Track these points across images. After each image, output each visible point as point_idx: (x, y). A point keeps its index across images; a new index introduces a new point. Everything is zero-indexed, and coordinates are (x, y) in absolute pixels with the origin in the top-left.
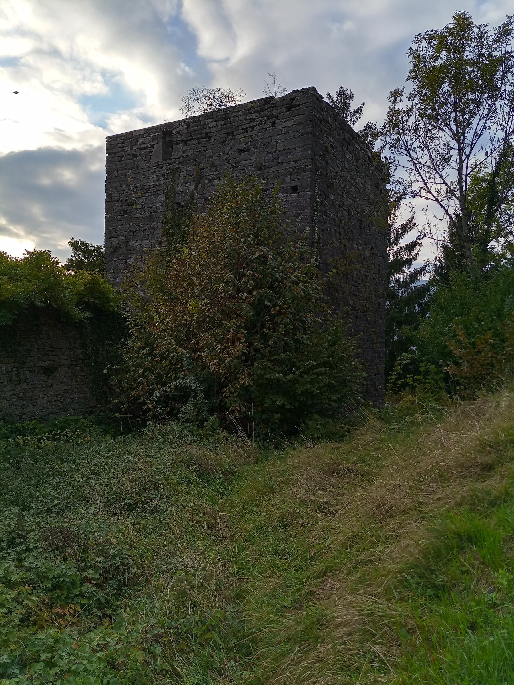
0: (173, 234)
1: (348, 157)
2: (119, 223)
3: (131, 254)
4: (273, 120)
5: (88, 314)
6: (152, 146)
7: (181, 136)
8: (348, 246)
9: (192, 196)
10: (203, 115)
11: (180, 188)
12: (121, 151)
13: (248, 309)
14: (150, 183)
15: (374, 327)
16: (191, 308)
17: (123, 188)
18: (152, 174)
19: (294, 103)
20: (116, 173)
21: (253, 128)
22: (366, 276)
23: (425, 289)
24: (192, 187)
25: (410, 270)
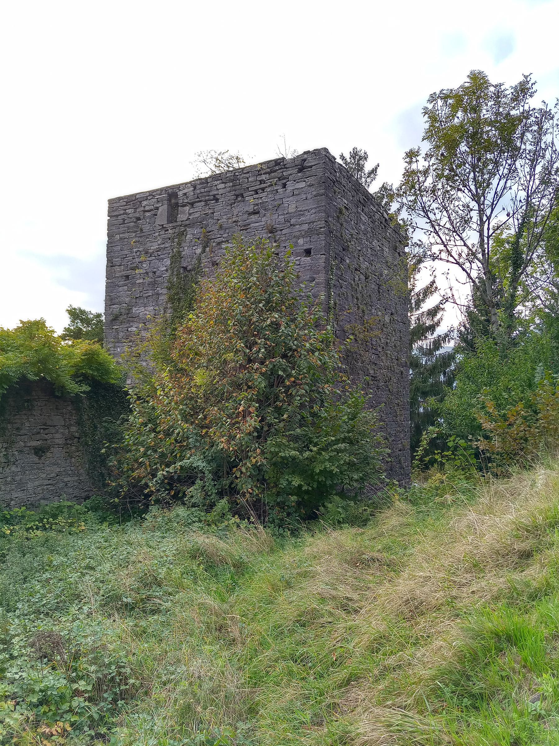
0: (179, 299)
1: (363, 219)
2: (121, 289)
3: (133, 321)
4: (284, 181)
6: (157, 208)
7: (187, 198)
8: (367, 312)
9: (199, 260)
11: (186, 251)
12: (124, 214)
13: (259, 380)
14: (155, 246)
15: (397, 399)
17: (126, 252)
19: (306, 164)
20: (118, 237)
21: (263, 189)
22: (387, 343)
24: (199, 251)
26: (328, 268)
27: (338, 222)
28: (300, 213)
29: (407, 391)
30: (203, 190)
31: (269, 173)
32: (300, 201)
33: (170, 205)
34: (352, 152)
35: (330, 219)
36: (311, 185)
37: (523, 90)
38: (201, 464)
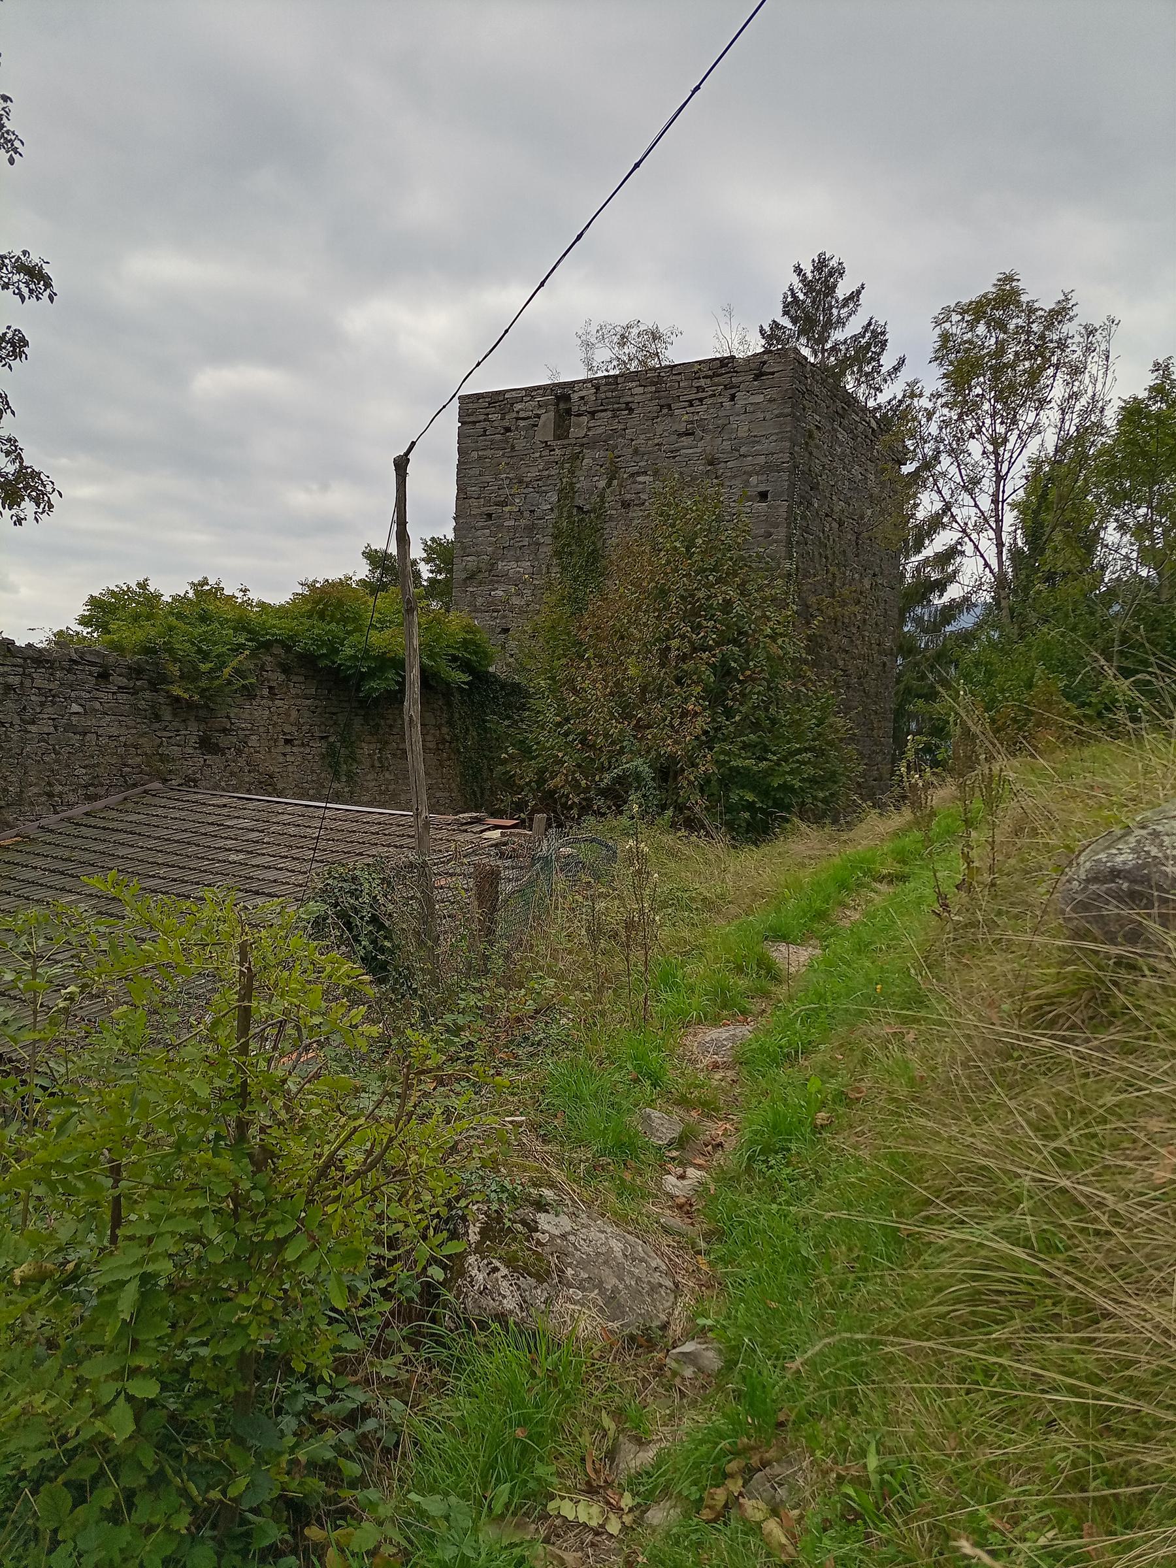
0: (571, 554)
1: (840, 436)
4: (733, 391)
8: (839, 576)
9: (602, 496)
10: (622, 375)
11: (582, 484)
12: (485, 420)
13: (708, 673)
15: (875, 703)
16: (632, 672)
17: (487, 478)
18: (535, 460)
19: (765, 369)
20: (475, 455)
21: (701, 400)
22: (865, 620)
23: (967, 637)
25: (942, 601)
26: (791, 518)
27: (806, 450)
28: (754, 440)
30: (609, 394)
31: (710, 377)
32: (754, 419)
33: (557, 411)
34: (816, 259)
35: (796, 449)
37: (1060, 313)
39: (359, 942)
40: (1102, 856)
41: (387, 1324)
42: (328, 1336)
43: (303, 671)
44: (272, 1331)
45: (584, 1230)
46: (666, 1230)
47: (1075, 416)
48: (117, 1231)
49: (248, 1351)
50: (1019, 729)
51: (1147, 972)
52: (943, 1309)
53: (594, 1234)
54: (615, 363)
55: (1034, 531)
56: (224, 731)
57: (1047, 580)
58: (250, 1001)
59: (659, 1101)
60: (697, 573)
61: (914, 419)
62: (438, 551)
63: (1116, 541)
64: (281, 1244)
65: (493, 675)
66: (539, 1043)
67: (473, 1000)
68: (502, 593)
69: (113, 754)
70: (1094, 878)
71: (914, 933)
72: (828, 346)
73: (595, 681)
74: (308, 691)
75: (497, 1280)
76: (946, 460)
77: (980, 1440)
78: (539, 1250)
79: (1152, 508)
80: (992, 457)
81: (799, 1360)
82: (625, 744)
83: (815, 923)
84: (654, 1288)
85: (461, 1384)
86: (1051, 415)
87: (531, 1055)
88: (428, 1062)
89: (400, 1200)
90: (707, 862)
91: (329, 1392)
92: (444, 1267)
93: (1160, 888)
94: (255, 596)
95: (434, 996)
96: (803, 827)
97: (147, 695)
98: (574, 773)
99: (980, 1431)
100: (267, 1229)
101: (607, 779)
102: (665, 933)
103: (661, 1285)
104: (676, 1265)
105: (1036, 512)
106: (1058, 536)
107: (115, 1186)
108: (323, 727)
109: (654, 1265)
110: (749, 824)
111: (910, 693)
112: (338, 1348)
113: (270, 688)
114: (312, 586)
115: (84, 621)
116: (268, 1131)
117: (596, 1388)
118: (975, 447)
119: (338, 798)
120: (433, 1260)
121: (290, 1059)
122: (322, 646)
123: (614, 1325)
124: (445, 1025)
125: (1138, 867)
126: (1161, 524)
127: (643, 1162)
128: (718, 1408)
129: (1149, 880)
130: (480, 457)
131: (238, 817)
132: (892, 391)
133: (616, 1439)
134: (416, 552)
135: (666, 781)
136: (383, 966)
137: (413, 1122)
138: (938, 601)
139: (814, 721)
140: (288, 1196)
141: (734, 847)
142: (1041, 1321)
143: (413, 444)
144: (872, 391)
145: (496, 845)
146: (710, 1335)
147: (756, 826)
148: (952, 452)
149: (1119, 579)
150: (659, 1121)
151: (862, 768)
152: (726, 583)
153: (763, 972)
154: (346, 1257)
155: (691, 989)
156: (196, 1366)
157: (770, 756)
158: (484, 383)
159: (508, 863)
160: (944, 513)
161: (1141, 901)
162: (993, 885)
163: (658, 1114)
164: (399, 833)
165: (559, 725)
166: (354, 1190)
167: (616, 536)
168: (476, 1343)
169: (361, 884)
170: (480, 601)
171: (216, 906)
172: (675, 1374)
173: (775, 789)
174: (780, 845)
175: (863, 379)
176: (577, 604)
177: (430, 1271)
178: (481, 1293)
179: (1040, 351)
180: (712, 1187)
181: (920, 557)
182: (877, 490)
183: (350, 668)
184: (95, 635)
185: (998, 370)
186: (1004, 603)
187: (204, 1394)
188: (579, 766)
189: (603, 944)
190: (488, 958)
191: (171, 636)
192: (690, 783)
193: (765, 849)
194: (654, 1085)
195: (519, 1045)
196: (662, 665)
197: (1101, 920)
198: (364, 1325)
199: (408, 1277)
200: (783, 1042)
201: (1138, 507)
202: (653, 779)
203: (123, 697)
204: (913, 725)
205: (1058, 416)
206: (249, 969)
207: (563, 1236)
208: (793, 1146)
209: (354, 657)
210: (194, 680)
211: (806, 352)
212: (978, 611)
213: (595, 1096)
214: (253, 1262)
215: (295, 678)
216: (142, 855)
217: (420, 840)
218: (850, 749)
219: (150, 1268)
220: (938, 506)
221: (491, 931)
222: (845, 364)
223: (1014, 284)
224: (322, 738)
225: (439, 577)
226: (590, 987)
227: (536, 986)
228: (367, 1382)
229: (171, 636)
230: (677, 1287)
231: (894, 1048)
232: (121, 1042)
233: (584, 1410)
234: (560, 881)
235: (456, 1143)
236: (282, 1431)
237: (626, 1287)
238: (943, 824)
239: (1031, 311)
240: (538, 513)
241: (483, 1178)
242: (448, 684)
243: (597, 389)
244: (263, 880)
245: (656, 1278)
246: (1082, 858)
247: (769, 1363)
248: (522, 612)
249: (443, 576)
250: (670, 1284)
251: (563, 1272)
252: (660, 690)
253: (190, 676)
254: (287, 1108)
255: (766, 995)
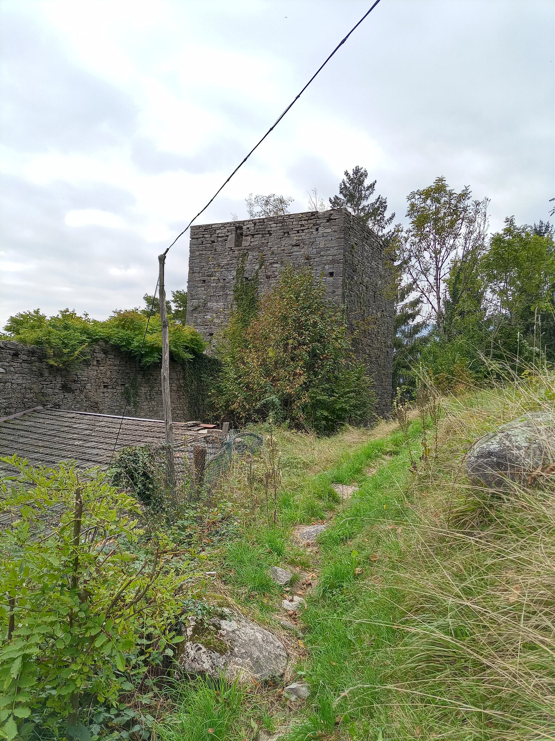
0: (242, 299)
1: (366, 248)
2: (199, 289)
3: (208, 312)
4: (317, 227)
5: (191, 356)
6: (228, 236)
7: (249, 231)
9: (257, 273)
11: (248, 267)
12: (202, 237)
13: (306, 355)
14: (225, 262)
16: (271, 354)
18: (226, 256)
19: (332, 217)
20: (198, 253)
21: (303, 230)
23: (425, 340)
24: (257, 267)
26: (344, 285)
28: (327, 249)
29: (390, 365)
32: (327, 239)
33: (236, 234)
36: (335, 231)
37: (464, 195)
38: (276, 400)
39: (137, 485)
40: (484, 445)
41: (146, 677)
42: (116, 684)
43: (114, 353)
44: (87, 682)
45: (244, 628)
46: (284, 628)
47: (471, 241)
48: (12, 633)
49: (75, 692)
50: (449, 383)
51: (506, 501)
52: (413, 665)
53: (248, 630)
54: (263, 213)
55: (454, 294)
56: (75, 381)
57: (460, 314)
58: (80, 518)
59: (281, 563)
60: (301, 309)
61: (399, 241)
62: (180, 298)
63: (491, 298)
64: (93, 639)
65: (205, 355)
66: (224, 535)
67: (192, 513)
68: (210, 317)
69: (19, 393)
70: (481, 456)
71: (402, 479)
72: (360, 208)
73: (253, 359)
74: (116, 363)
75: (200, 654)
76: (414, 260)
77: (431, 729)
78: (221, 639)
79: (506, 282)
80: (434, 259)
81: (347, 692)
82: (267, 388)
83: (356, 474)
84: (277, 657)
85: (182, 707)
86: (460, 241)
87: (220, 541)
88: (167, 547)
89: (152, 616)
90: (305, 445)
91: (116, 712)
92: (174, 650)
93: (510, 461)
94: (91, 317)
95: (173, 511)
96: (350, 428)
97: (37, 364)
98: (243, 402)
99: (431, 725)
100: (86, 631)
101: (259, 405)
102: (285, 480)
103: (280, 655)
104: (288, 645)
105: (455, 284)
106: (465, 295)
107: (11, 610)
108: (123, 380)
109: (277, 645)
110: (325, 427)
111: (399, 365)
112: (122, 690)
113: (97, 361)
114: (119, 313)
115: (8, 329)
116: (88, 582)
117: (248, 707)
118: (426, 254)
119: (129, 414)
120: (168, 646)
121: (101, 543)
122: (123, 341)
123: (258, 676)
124: (178, 526)
125: (501, 451)
126: (511, 290)
127: (273, 594)
128: (307, 716)
129: (505, 457)
130: (200, 254)
131: (80, 423)
132: (389, 229)
133: (258, 733)
134: (169, 297)
135: (287, 406)
136: (149, 497)
137: (160, 576)
138: (412, 323)
139: (355, 378)
140: (97, 614)
141: (319, 438)
142: (459, 670)
143: (168, 249)
144: (380, 228)
145: (205, 438)
146: (304, 679)
147: (329, 426)
148: (416, 256)
149: (492, 315)
150: (281, 573)
151: (377, 400)
152: (314, 314)
153: (331, 499)
154: (125, 644)
155: (297, 507)
156: (50, 700)
157: (335, 394)
158: (201, 221)
159: (211, 446)
160: (414, 283)
161: (502, 467)
162: (437, 457)
163: (280, 569)
164: (158, 430)
165: (236, 379)
166: (128, 611)
167: (264, 292)
168: (190, 686)
169: (139, 457)
170: (199, 320)
171: (65, 471)
172: (287, 699)
173: (337, 410)
174: (340, 437)
175: (376, 223)
176: (245, 323)
177: (167, 651)
178: (192, 661)
179: (455, 212)
180: (306, 606)
181: (403, 303)
182: (383, 273)
183: (136, 351)
184: (13, 335)
185: (436, 220)
186: (441, 325)
187: (53, 714)
188: (245, 399)
189: (255, 485)
190: (200, 492)
191: (49, 336)
192: (298, 407)
193: (333, 438)
194: (279, 555)
195: (214, 535)
196: (285, 351)
197: (485, 476)
198: (134, 678)
199: (157, 653)
200: (340, 533)
201: (500, 282)
202: (280, 405)
203: (25, 365)
204: (401, 380)
205: (464, 241)
206: (80, 502)
207: (233, 632)
208: (344, 585)
209: (139, 346)
210: (60, 357)
211: (350, 210)
212: (430, 328)
213: (250, 560)
214: (79, 648)
215: (110, 356)
216: (32, 442)
217: (168, 435)
218: (372, 391)
219: (27, 652)
220: (411, 280)
221: (201, 480)
222: (368, 215)
223: (443, 182)
224: (122, 385)
225: (180, 309)
226: (249, 506)
227: (223, 506)
228: (136, 706)
229: (49, 336)
230: (288, 656)
231: (392, 535)
232: (16, 539)
233: (242, 718)
234: (235, 454)
235: (182, 586)
236: (92, 732)
237: (264, 656)
238: (415, 427)
239: (451, 194)
240: (227, 280)
241: (194, 603)
242: (183, 360)
243: (255, 224)
244: (91, 454)
245: (278, 651)
246: (475, 446)
247: (332, 693)
248: (219, 326)
249: (182, 309)
250: (285, 655)
251: (233, 650)
252: (284, 363)
253: (58, 355)
254: (98, 571)
255: (332, 509)
